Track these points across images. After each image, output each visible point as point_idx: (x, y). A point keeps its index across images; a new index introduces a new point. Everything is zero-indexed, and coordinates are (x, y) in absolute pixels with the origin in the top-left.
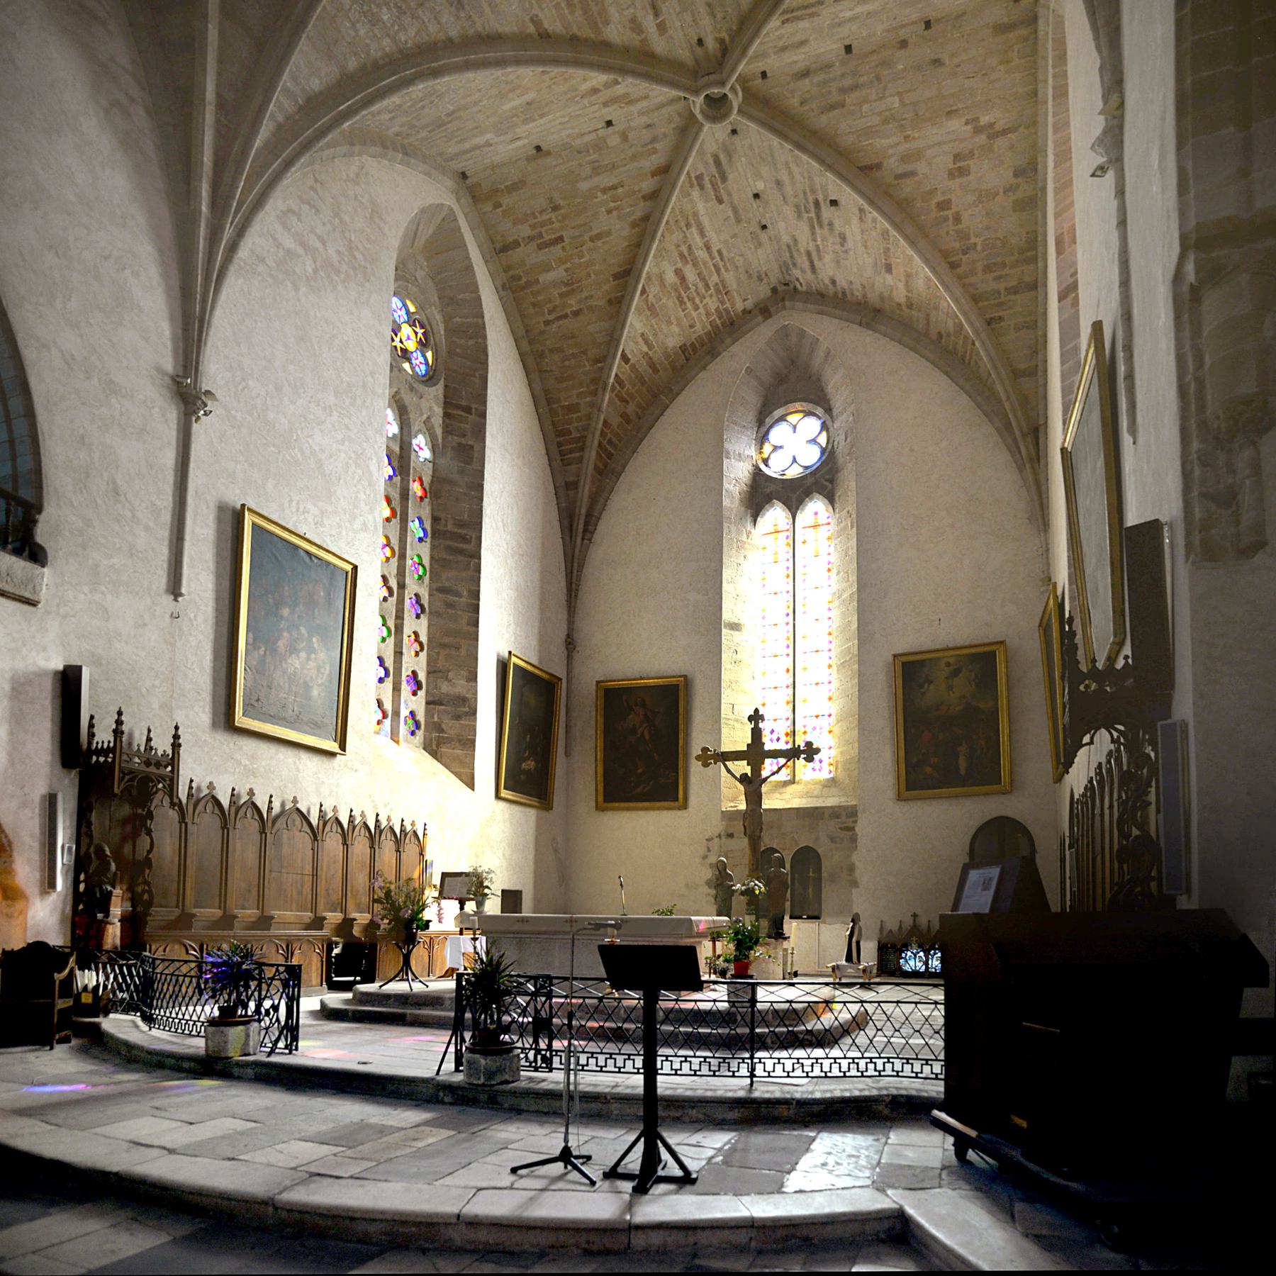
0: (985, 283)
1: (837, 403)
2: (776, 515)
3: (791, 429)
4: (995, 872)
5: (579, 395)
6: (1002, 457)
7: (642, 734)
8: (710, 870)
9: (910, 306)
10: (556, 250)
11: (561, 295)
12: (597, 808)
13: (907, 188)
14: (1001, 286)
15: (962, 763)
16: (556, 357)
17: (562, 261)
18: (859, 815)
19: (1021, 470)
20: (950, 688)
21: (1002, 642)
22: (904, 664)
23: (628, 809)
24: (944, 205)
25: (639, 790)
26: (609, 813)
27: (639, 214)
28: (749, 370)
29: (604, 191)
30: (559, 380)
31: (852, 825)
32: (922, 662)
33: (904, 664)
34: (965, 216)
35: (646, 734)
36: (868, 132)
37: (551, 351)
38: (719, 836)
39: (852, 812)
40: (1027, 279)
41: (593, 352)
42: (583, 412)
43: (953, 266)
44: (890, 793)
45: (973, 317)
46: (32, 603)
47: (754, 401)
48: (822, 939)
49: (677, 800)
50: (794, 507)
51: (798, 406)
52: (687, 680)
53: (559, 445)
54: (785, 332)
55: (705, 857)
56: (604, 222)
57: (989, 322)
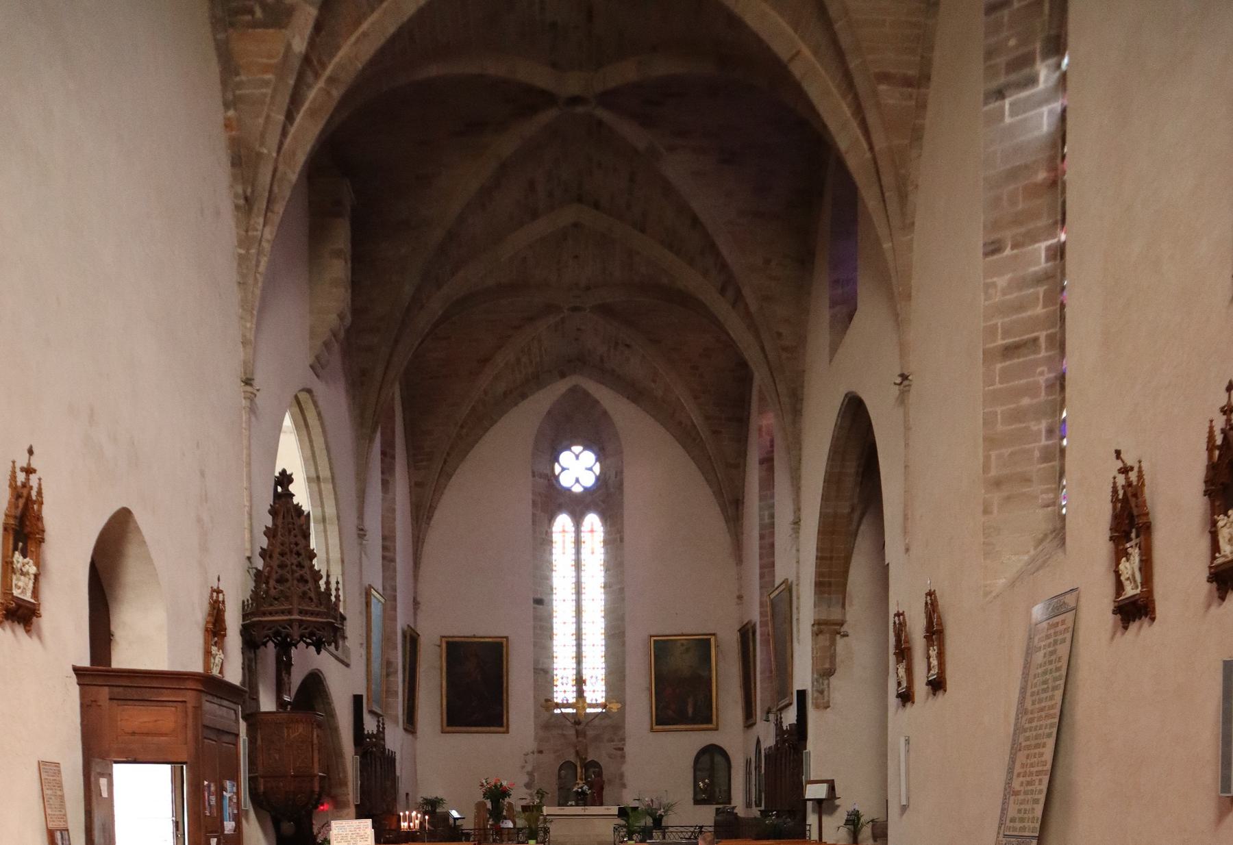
3: (589, 466)
6: (715, 510)
8: (527, 776)
15: (690, 711)
18: (627, 740)
21: (714, 634)
31: (622, 747)
38: (533, 753)
44: (647, 725)
48: (1068, 596)
52: (507, 732)
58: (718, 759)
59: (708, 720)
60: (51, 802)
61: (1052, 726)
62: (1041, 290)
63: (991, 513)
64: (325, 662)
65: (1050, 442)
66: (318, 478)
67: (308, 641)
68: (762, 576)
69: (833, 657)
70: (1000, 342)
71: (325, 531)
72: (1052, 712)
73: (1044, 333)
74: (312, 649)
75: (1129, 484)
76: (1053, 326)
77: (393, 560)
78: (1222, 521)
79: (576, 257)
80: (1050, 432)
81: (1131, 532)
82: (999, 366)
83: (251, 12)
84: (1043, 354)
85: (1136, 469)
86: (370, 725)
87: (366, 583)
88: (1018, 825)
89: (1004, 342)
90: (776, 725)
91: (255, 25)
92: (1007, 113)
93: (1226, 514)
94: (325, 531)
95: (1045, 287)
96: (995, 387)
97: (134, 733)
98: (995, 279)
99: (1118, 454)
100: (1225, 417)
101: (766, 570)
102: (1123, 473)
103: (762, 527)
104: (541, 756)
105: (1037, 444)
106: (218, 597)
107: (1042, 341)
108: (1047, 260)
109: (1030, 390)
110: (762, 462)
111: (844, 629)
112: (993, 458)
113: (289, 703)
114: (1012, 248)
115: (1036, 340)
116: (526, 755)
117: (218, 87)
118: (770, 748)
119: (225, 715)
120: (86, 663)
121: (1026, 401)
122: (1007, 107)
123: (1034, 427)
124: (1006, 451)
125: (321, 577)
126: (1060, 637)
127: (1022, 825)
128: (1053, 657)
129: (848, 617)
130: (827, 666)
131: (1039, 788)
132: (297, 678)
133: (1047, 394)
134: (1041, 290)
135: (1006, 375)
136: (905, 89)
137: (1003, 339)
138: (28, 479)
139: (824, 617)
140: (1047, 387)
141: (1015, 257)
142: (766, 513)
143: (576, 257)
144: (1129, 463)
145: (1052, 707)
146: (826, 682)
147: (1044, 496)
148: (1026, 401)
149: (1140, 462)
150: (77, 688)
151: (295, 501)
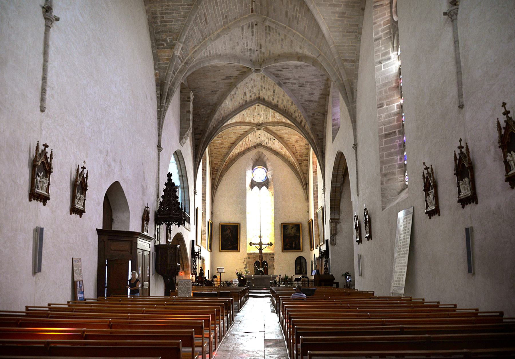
0: (299, 158)
1: (269, 169)
2: (256, 188)
4: (315, 271)
5: (218, 162)
6: (300, 187)
7: (230, 236)
9: (285, 155)
10: (221, 138)
11: (219, 145)
12: (220, 251)
13: (288, 142)
14: (302, 159)
15: (294, 246)
16: (215, 154)
17: (221, 140)
19: (304, 190)
20: (292, 231)
21: (301, 223)
22: (283, 225)
23: (231, 252)
24: (293, 145)
25: (229, 248)
26: (222, 252)
27: (239, 136)
28: (251, 159)
29: (234, 132)
30: (214, 158)
32: (286, 225)
33: (283, 225)
34: (297, 147)
35: (231, 235)
36: (282, 134)
37: (214, 153)
38: (247, 258)
39: (273, 254)
40: (306, 159)
41: (223, 155)
42: (218, 165)
43: (294, 154)
45: (297, 163)
46: (190, 231)
47: (252, 164)
49: (237, 250)
50: (260, 188)
51: (261, 166)
53: (212, 170)
54: (259, 152)
55: (244, 263)
56: (232, 136)
57: (300, 164)
58: (303, 261)
59: (300, 249)
60: (76, 271)
61: (407, 250)
62: (396, 117)
63: (383, 184)
64: (181, 229)
65: (401, 162)
66: (182, 176)
67: (176, 223)
68: (314, 206)
69: (336, 230)
70: (384, 133)
71: (184, 191)
72: (407, 246)
73: (398, 130)
74: (177, 226)
75: (428, 173)
76: (400, 128)
77: (205, 200)
78: (461, 183)
79: (259, 114)
80: (401, 159)
81: (430, 188)
82: (384, 140)
83: (163, 45)
84: (397, 136)
85: (430, 168)
86: (196, 249)
87: (196, 207)
88: (397, 283)
89: (385, 133)
90: (320, 250)
91: (165, 48)
92: (382, 68)
93: (462, 181)
94: (184, 191)
95: (397, 116)
96: (383, 146)
97: (115, 250)
98: (381, 115)
99: (424, 163)
100: (460, 150)
101: (316, 204)
102: (426, 169)
103: (314, 191)
104: (249, 259)
105: (397, 163)
106: (147, 209)
107: (397, 132)
108: (397, 109)
109: (394, 147)
110: (313, 172)
111: (340, 221)
112: (383, 167)
113: (170, 242)
114: (386, 106)
115: (395, 132)
116: (244, 259)
117: (153, 64)
118: (318, 257)
119: (146, 245)
120: (101, 227)
121: (393, 150)
122: (382, 66)
123: (395, 157)
124: (387, 166)
125: (180, 204)
126: (408, 222)
127: (399, 283)
128: (406, 228)
129: (340, 217)
130: (335, 232)
131: (404, 271)
132: (173, 235)
133: (399, 148)
134: (396, 117)
135: (386, 143)
136: (352, 64)
137: (385, 132)
138: (83, 171)
139: (333, 217)
140: (399, 146)
141: (387, 108)
142: (315, 187)
143: (259, 114)
144: (428, 166)
145: (407, 244)
146: (334, 237)
147: (400, 179)
148: (393, 150)
149: (431, 166)
150: (97, 235)
151: (172, 182)
